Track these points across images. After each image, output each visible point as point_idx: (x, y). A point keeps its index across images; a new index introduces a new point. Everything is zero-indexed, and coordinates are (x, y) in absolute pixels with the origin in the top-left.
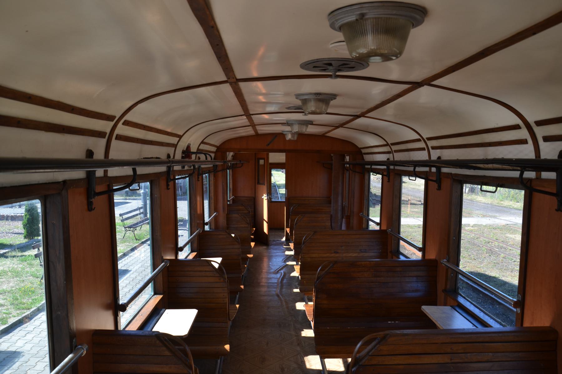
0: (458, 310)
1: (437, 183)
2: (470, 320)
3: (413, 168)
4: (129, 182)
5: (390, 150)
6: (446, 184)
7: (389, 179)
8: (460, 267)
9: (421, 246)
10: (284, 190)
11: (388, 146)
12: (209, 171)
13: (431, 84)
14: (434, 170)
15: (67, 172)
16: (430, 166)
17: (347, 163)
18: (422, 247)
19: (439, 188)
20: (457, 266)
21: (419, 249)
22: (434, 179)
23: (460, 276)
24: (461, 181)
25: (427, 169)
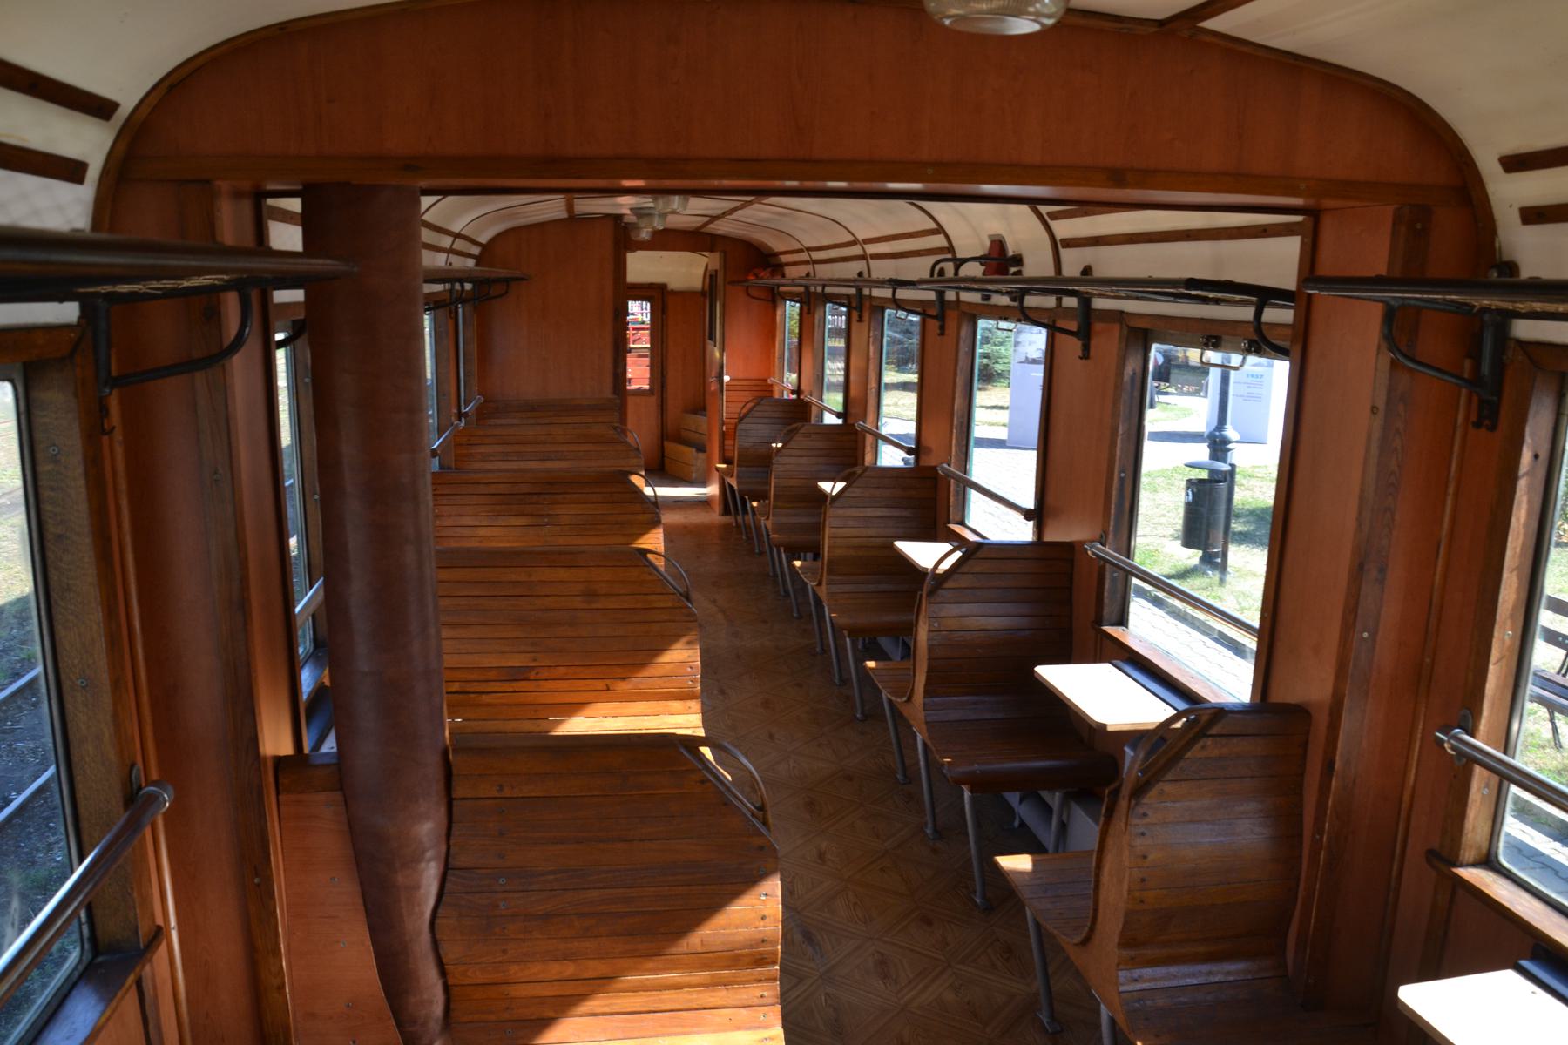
0: (1027, 632)
1: (1079, 340)
2: (1166, 699)
3: (890, 291)
4: (694, 450)
5: (865, 246)
6: (1107, 342)
7: (942, 328)
8: (1136, 558)
9: (1030, 503)
10: (916, 376)
11: (940, 233)
12: (435, 304)
13: (1202, 28)
14: (1071, 302)
15: (79, 795)
16: (1060, 293)
17: (462, 286)
18: (1035, 510)
19: (1086, 355)
20: (1128, 558)
21: (1028, 515)
22: (1073, 326)
23: (1135, 581)
24: (1141, 335)
25: (1050, 302)
